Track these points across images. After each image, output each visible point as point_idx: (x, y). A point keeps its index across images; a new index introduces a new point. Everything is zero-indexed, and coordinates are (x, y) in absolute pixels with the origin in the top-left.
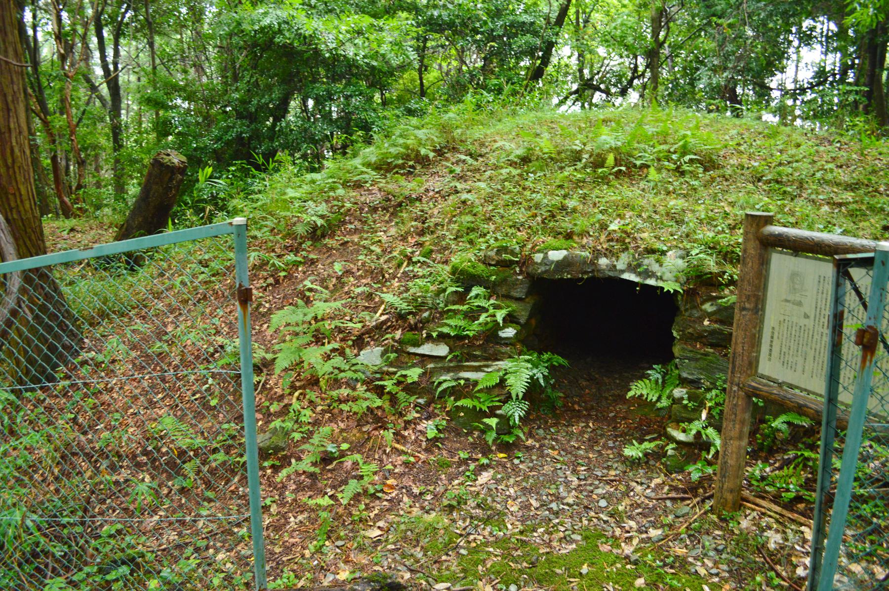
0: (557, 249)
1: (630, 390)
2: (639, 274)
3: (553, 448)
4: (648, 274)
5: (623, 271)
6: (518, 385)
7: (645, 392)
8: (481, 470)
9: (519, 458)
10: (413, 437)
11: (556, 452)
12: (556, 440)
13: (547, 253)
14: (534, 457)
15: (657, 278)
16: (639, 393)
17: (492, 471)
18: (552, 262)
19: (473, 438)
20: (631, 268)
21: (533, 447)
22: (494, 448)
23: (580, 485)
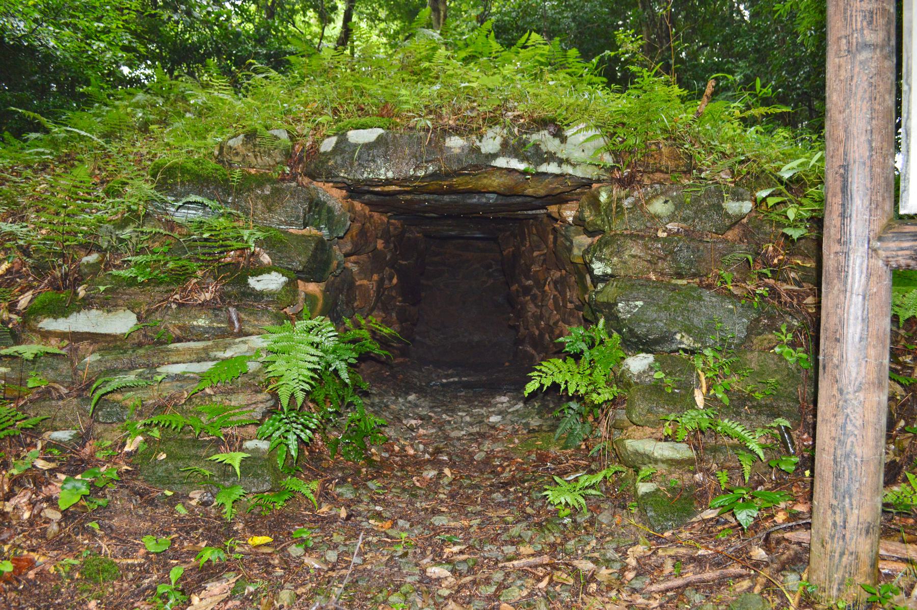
0: (364, 127)
1: (530, 379)
2: (523, 158)
3: (379, 516)
4: (540, 156)
5: (495, 156)
6: (293, 375)
7: (559, 379)
8: (202, 580)
9: (303, 541)
10: (26, 515)
11: (388, 524)
12: (386, 504)
13: (344, 135)
14: (337, 538)
15: (561, 162)
16: (547, 382)
17: (231, 579)
18: (356, 145)
19: (187, 507)
20: (506, 149)
21: (335, 518)
22: (239, 526)
23: (461, 587)
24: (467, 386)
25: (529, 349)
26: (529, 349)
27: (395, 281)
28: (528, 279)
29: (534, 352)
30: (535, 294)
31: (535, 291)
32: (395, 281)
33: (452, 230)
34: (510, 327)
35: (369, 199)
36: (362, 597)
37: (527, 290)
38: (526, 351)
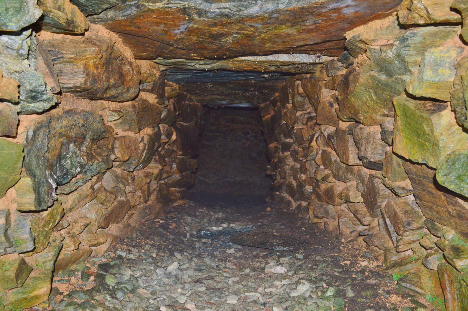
24: (236, 238)
25: (286, 195)
26: (286, 195)
27: (174, 137)
28: (287, 136)
29: (290, 199)
30: (295, 150)
31: (295, 147)
32: (174, 137)
33: (223, 100)
34: (268, 176)
35: (112, 19)
36: (290, 3)
37: (286, 147)
38: (283, 197)
